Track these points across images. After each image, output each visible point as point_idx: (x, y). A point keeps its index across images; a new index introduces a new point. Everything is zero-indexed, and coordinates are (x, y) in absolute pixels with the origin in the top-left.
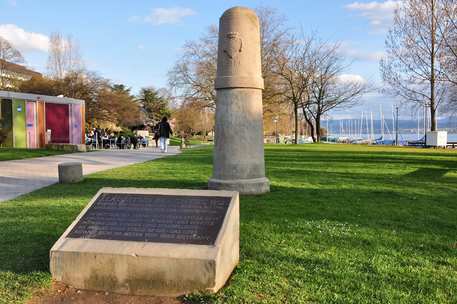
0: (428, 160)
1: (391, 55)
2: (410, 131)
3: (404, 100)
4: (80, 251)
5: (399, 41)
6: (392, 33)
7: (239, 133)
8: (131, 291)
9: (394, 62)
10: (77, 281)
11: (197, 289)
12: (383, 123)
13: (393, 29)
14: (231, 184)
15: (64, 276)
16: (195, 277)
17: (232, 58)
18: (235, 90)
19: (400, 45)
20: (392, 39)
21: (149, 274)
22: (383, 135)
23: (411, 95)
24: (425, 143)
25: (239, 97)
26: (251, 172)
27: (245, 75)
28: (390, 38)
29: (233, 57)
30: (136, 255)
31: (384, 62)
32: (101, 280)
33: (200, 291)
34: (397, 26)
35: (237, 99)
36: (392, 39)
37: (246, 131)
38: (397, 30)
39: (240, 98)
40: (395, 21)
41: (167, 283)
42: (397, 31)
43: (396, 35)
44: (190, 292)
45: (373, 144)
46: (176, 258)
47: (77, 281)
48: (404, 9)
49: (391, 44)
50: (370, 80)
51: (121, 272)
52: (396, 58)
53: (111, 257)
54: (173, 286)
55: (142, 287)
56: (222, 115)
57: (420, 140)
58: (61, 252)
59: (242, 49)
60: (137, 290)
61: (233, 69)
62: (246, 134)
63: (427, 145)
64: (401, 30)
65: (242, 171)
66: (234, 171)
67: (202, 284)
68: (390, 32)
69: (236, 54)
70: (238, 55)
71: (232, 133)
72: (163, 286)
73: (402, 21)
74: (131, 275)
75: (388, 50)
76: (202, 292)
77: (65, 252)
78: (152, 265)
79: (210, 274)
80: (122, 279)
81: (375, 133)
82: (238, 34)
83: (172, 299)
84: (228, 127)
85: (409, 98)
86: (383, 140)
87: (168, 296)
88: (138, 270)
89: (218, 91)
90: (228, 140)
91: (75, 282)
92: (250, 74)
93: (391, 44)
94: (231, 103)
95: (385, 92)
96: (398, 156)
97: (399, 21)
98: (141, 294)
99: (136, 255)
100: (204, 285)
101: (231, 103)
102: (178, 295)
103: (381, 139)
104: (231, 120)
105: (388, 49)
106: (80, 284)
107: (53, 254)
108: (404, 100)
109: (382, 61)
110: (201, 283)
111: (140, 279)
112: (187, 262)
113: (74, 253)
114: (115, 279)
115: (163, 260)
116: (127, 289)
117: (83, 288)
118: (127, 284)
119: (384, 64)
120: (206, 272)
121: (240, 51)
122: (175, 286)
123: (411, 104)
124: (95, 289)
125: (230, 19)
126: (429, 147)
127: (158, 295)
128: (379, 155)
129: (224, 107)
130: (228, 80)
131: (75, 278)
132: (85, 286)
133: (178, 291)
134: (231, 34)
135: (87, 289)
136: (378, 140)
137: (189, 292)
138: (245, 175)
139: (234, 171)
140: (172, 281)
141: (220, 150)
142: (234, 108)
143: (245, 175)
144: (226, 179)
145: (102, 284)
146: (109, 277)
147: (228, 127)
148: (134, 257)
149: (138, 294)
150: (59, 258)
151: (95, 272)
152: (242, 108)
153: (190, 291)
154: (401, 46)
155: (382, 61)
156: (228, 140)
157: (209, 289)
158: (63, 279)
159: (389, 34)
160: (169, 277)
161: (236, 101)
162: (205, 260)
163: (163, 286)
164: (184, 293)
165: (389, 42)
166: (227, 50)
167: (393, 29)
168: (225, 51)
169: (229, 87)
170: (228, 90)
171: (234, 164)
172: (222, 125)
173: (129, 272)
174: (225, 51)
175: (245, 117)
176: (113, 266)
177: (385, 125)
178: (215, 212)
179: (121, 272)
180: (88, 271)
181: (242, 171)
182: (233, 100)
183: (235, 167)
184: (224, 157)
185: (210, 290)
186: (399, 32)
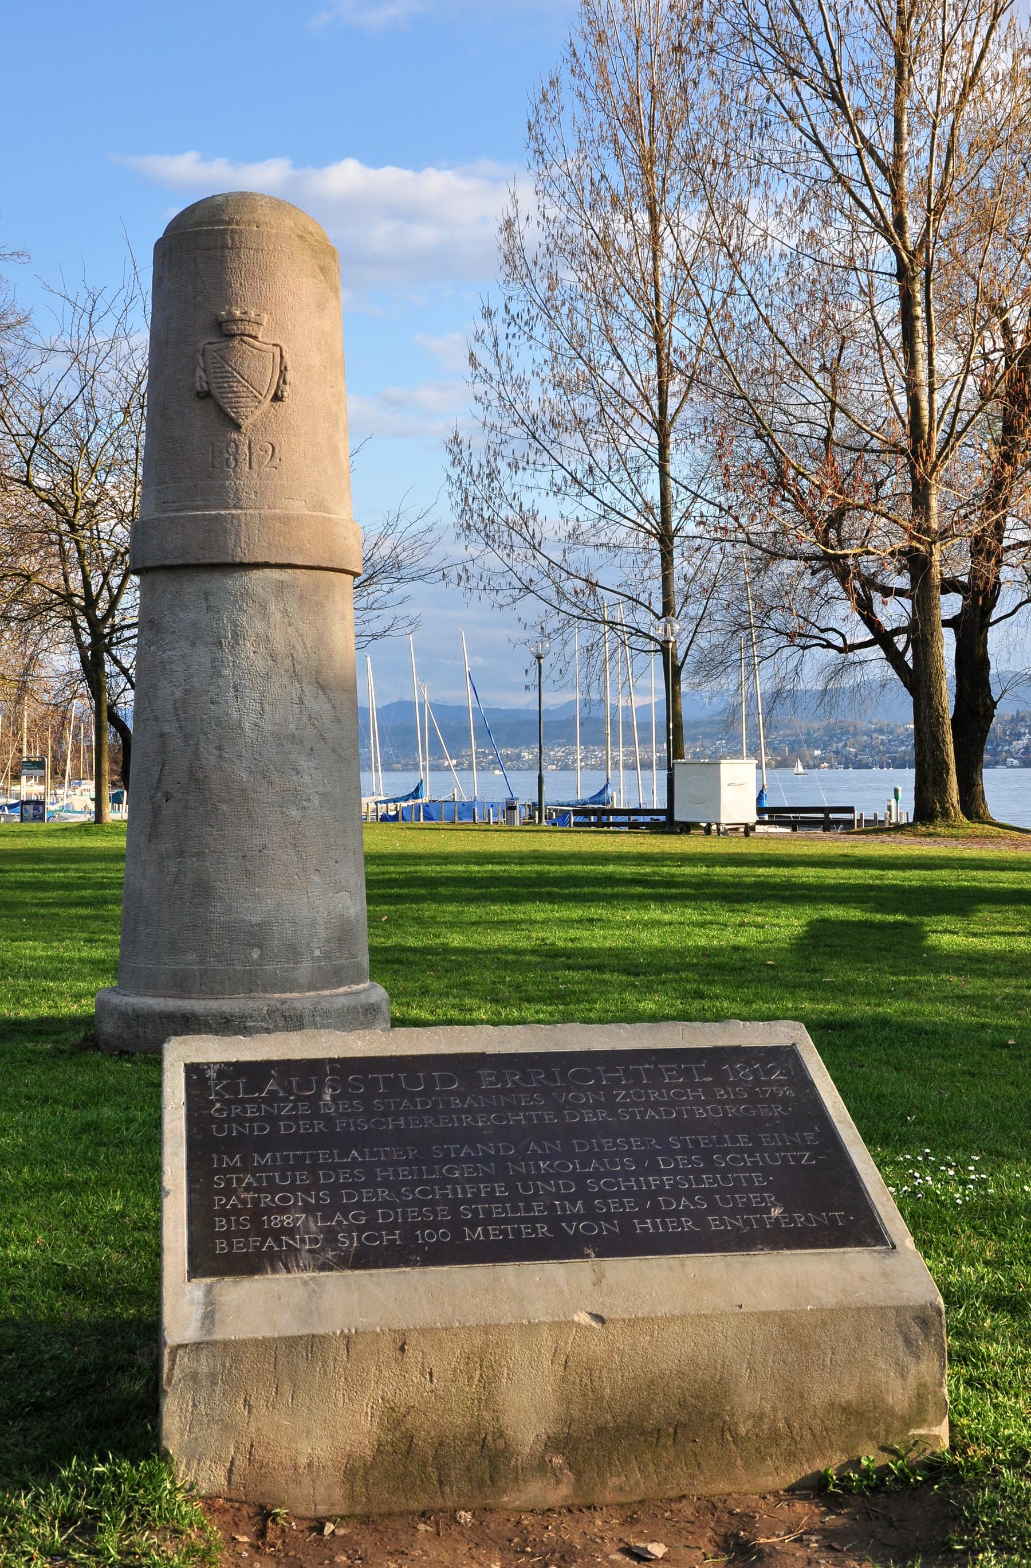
0: (774, 886)
1: (493, 419)
2: (519, 757)
3: (555, 622)
4: (319, 1331)
5: (527, 358)
6: (497, 320)
7: (275, 776)
8: (575, 1492)
9: (506, 451)
10: (306, 1481)
11: (872, 1437)
12: (423, 722)
13: (497, 304)
14: (243, 1017)
15: (241, 1463)
16: (860, 1387)
17: (238, 427)
18: (256, 574)
19: (528, 376)
20: (496, 344)
21: (660, 1398)
22: (426, 777)
23: (582, 602)
24: (669, 812)
25: (272, 607)
26: (327, 956)
27: (298, 507)
28: (490, 342)
29: (245, 424)
30: (598, 1318)
31: (464, 446)
32: (430, 1454)
33: (883, 1449)
34: (515, 289)
35: (266, 616)
36: (496, 344)
37: (304, 763)
38: (515, 308)
39: (278, 615)
40: (507, 268)
41: (742, 1430)
42: (514, 312)
43: (513, 329)
44: (845, 1459)
45: (385, 818)
46: (775, 1313)
47: (306, 1481)
48: (543, 222)
49: (494, 370)
50: (421, 525)
51: (528, 1409)
52: (514, 431)
53: (478, 1341)
54: (771, 1441)
55: (628, 1461)
56: (187, 692)
57: (593, 800)
58: (226, 1344)
59: (287, 391)
60: (604, 1483)
61: (246, 479)
62: (307, 778)
63: (676, 818)
64: (534, 312)
65: (293, 952)
66: (255, 954)
67: (893, 1415)
68: (488, 314)
69: (258, 413)
70: (266, 415)
71: (245, 776)
72: (723, 1443)
73: (537, 275)
74: (576, 1414)
75: (480, 393)
76: (894, 1452)
77: (244, 1343)
78: (672, 1353)
79: (923, 1367)
80: (531, 1439)
81: (387, 767)
82: (265, 318)
83: (771, 1499)
84: (220, 748)
85: (576, 612)
86: (425, 799)
87: (746, 1487)
88: (606, 1383)
89: (149, 577)
90: (225, 807)
91: (297, 1482)
92: (320, 505)
93: (494, 370)
94: (235, 635)
95: (473, 583)
96: (648, 870)
97: (524, 272)
98: (622, 1499)
99: (598, 1318)
100: (902, 1417)
101: (235, 635)
102: (792, 1478)
103: (416, 794)
104: (235, 715)
105: (480, 388)
106: (321, 1491)
107: (184, 1360)
108: (555, 622)
109: (456, 440)
110: (890, 1412)
111: (618, 1429)
112: (824, 1322)
113: (292, 1342)
114: (501, 1444)
115: (718, 1327)
116: (558, 1482)
117: (340, 1509)
118: (558, 1460)
119: (465, 454)
120: (908, 1360)
121: (277, 398)
122: (775, 1437)
123: (580, 636)
124: (399, 1502)
125: (224, 247)
126: (686, 828)
127: (704, 1490)
128: (497, 868)
129: (201, 655)
130: (225, 531)
131: (295, 1467)
132: (351, 1497)
133: (791, 1457)
134: (235, 321)
135: (358, 1510)
136: (406, 798)
137: (838, 1459)
138: (305, 969)
139: (255, 954)
140: (762, 1416)
141: (181, 853)
142: (251, 655)
143: (305, 969)
144: (214, 994)
145: (435, 1477)
146: (470, 1438)
147: (220, 748)
148: (588, 1328)
149: (609, 1496)
150: (213, 1376)
151: (398, 1423)
152: (288, 662)
153: (844, 1450)
154: (535, 382)
155: (456, 440)
156: (225, 807)
157: (922, 1431)
158: (236, 1478)
159: (482, 324)
160: (752, 1398)
161: (260, 626)
162: (899, 1310)
163: (723, 1443)
164: (819, 1465)
165: (485, 358)
166: (216, 392)
167: (497, 304)
168: (206, 396)
169: (229, 560)
170: (205, 577)
171: (255, 919)
172: (187, 737)
173: (566, 1400)
174: (206, 396)
175: (301, 701)
176: (489, 1383)
177: (432, 729)
178: (778, 1110)
179: (528, 1409)
180: (365, 1424)
181: (293, 952)
182: (244, 620)
183: (257, 936)
184: (203, 890)
185: (927, 1436)
186: (526, 316)
